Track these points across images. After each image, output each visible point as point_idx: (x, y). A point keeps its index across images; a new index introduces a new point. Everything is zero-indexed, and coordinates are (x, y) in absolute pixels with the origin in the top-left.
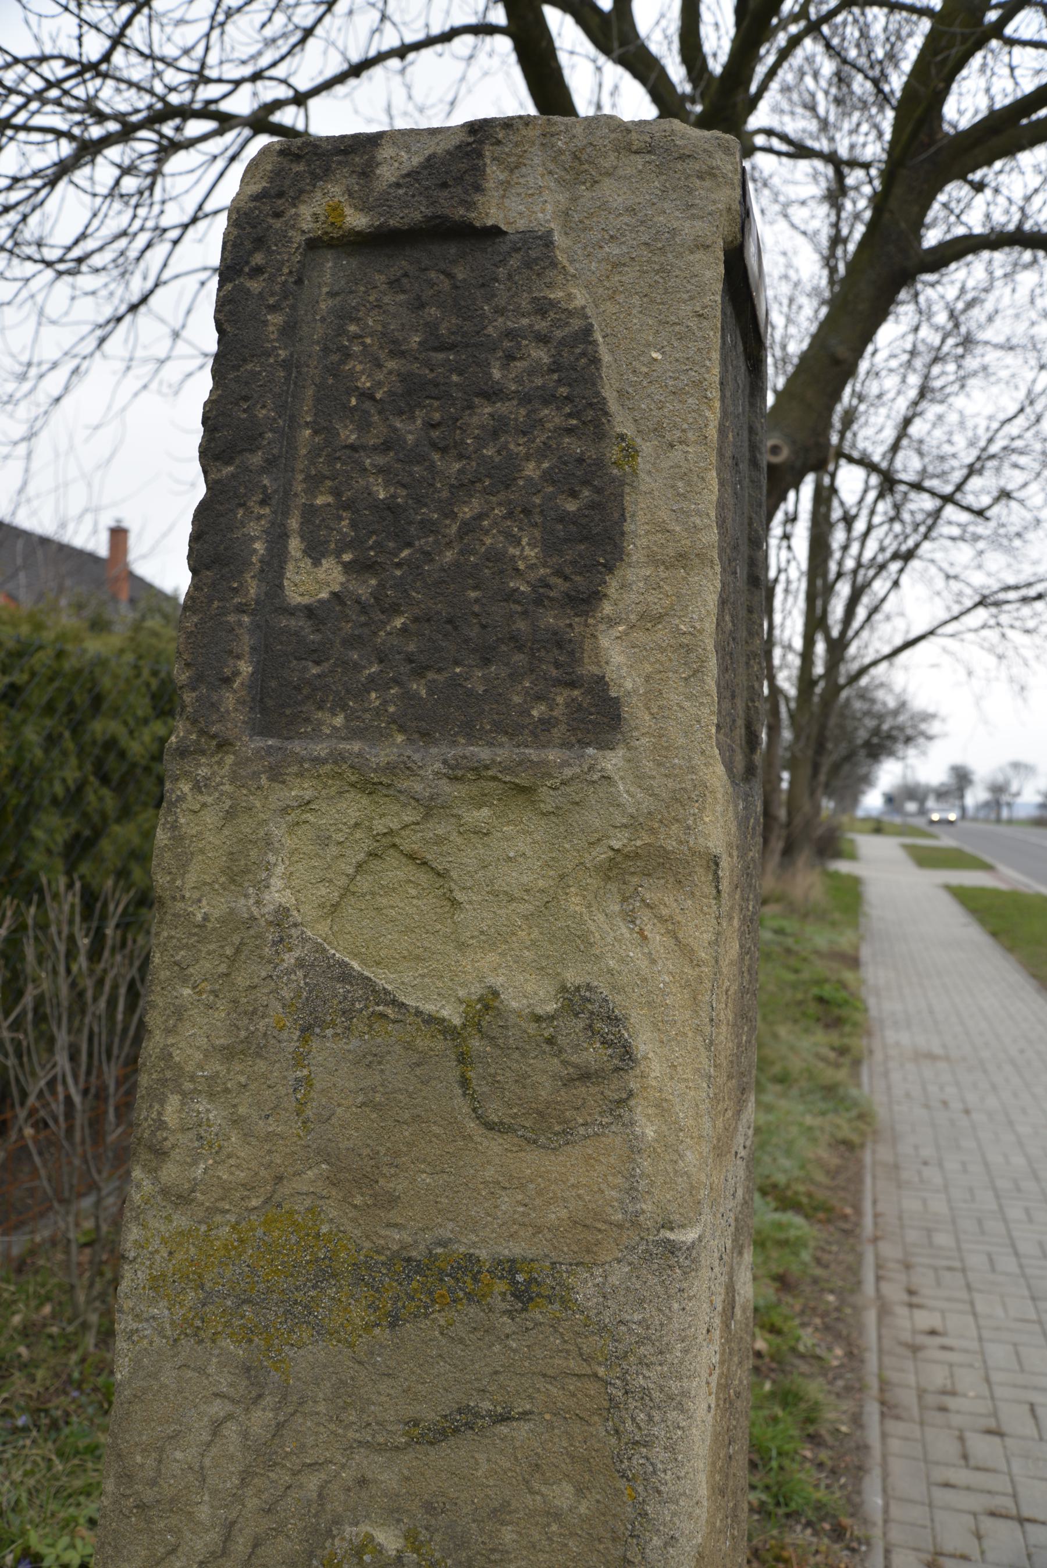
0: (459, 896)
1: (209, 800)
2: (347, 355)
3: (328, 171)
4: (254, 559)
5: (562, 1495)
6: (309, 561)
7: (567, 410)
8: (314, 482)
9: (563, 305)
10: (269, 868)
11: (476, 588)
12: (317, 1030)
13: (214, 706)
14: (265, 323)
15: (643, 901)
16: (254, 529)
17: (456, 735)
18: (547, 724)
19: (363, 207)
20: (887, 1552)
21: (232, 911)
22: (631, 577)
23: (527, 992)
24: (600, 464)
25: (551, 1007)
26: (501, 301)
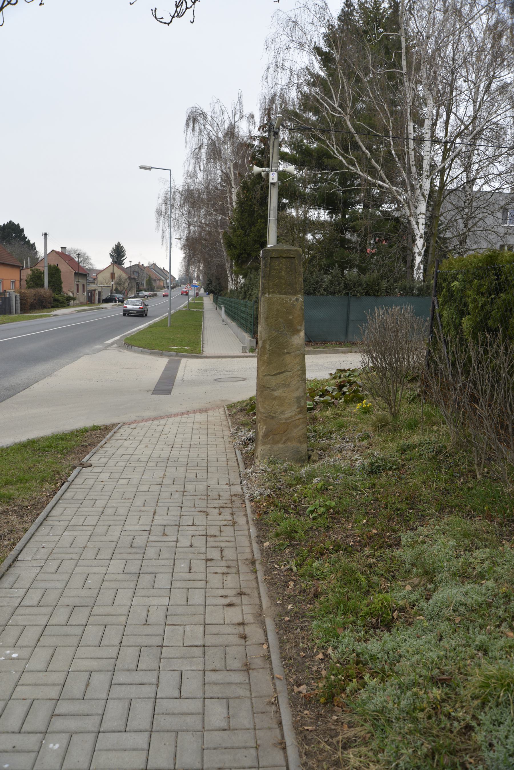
20: (248, 521)
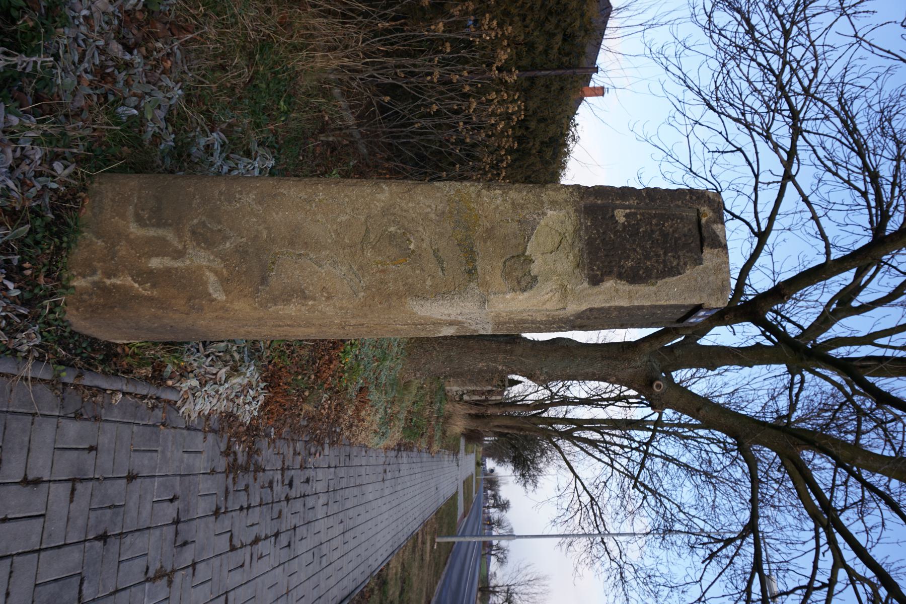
5: (429, 282)
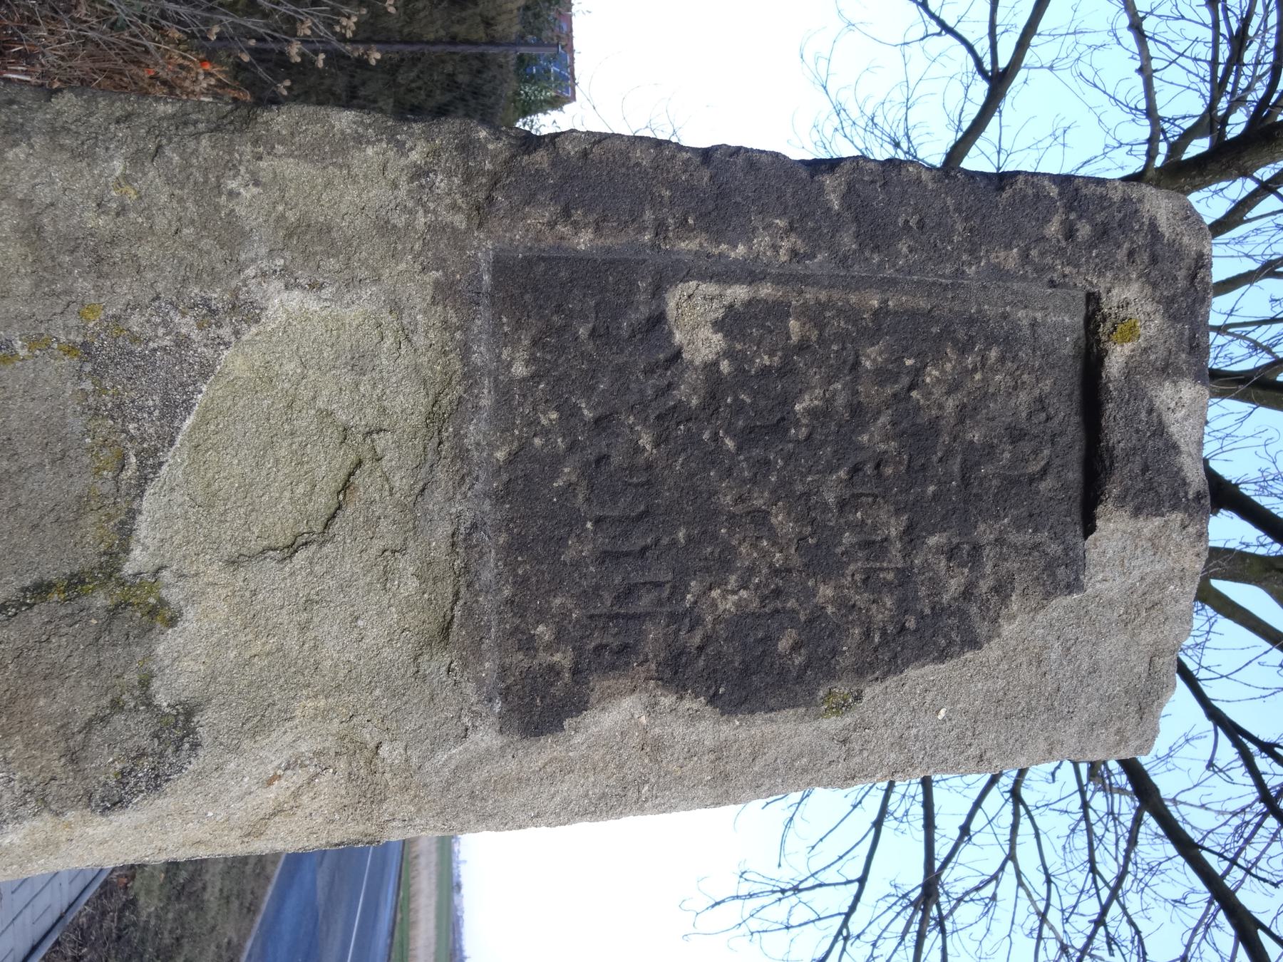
0: (301, 555)
1: (402, 193)
2: (963, 350)
3: (1173, 318)
4: (723, 247)
6: (720, 314)
7: (890, 629)
8: (814, 315)
9: (1004, 612)
10: (315, 286)
11: (689, 539)
12: (88, 368)
13: (530, 200)
14: (1008, 247)
15: (317, 775)
16: (762, 242)
17: (509, 530)
18: (528, 645)
19: (1130, 371)
21: (245, 235)
22: (702, 726)
23: (182, 660)
24: (831, 675)
25: (162, 700)
26: (1014, 537)
